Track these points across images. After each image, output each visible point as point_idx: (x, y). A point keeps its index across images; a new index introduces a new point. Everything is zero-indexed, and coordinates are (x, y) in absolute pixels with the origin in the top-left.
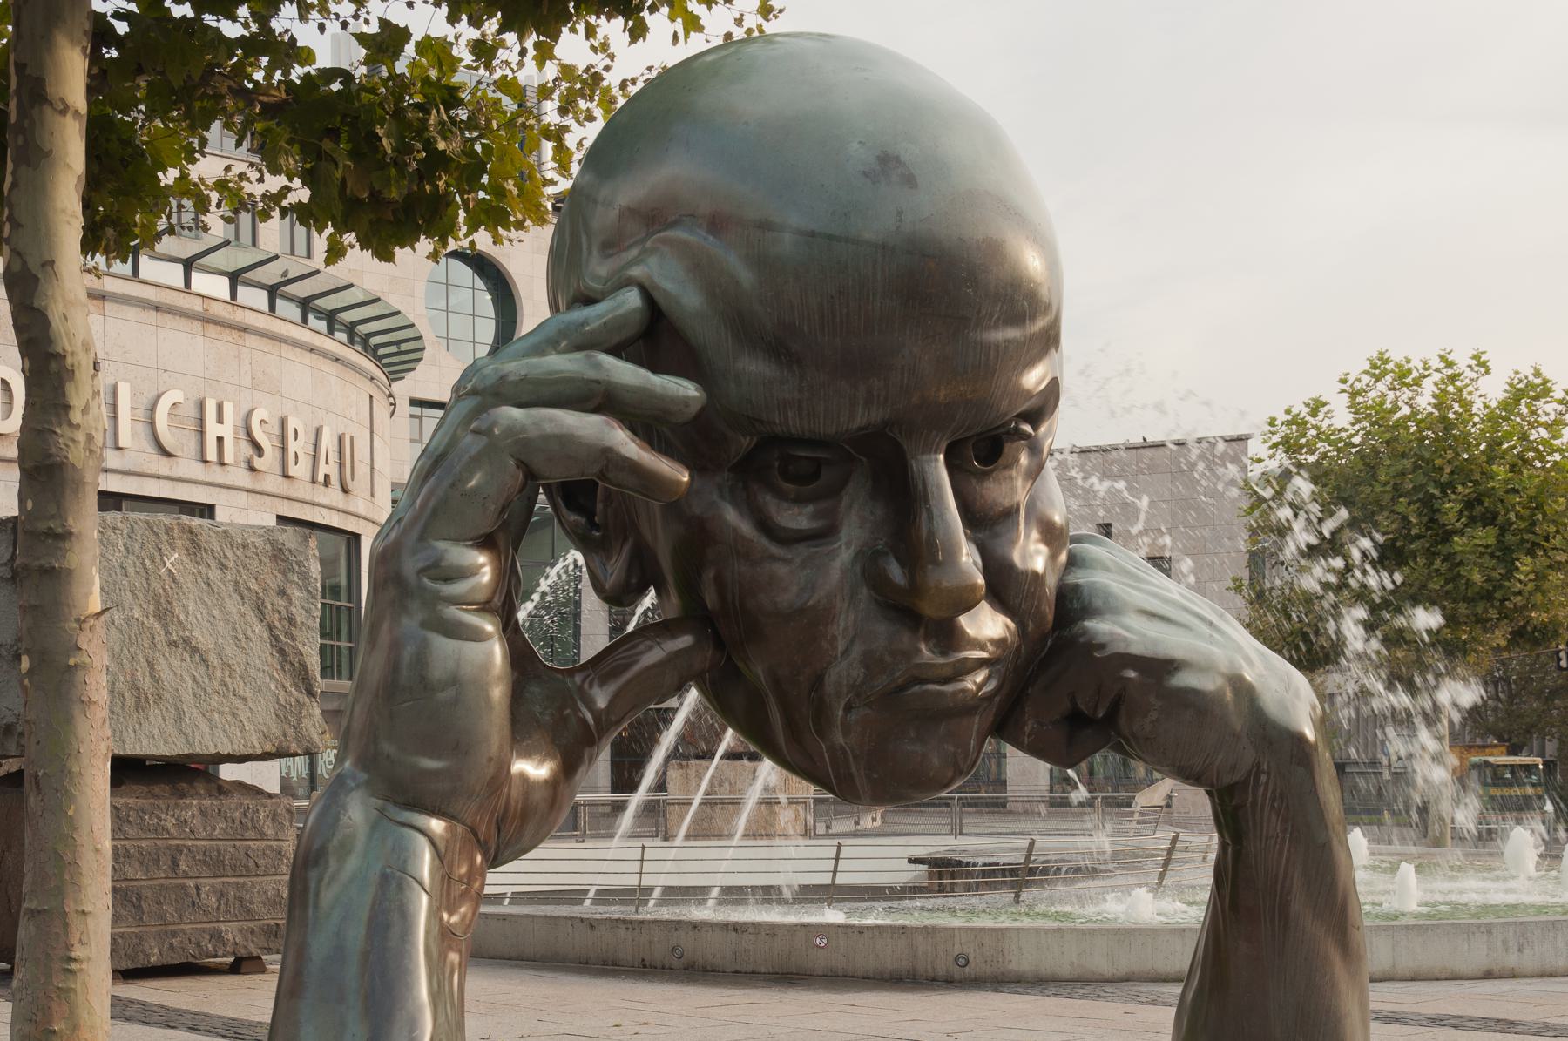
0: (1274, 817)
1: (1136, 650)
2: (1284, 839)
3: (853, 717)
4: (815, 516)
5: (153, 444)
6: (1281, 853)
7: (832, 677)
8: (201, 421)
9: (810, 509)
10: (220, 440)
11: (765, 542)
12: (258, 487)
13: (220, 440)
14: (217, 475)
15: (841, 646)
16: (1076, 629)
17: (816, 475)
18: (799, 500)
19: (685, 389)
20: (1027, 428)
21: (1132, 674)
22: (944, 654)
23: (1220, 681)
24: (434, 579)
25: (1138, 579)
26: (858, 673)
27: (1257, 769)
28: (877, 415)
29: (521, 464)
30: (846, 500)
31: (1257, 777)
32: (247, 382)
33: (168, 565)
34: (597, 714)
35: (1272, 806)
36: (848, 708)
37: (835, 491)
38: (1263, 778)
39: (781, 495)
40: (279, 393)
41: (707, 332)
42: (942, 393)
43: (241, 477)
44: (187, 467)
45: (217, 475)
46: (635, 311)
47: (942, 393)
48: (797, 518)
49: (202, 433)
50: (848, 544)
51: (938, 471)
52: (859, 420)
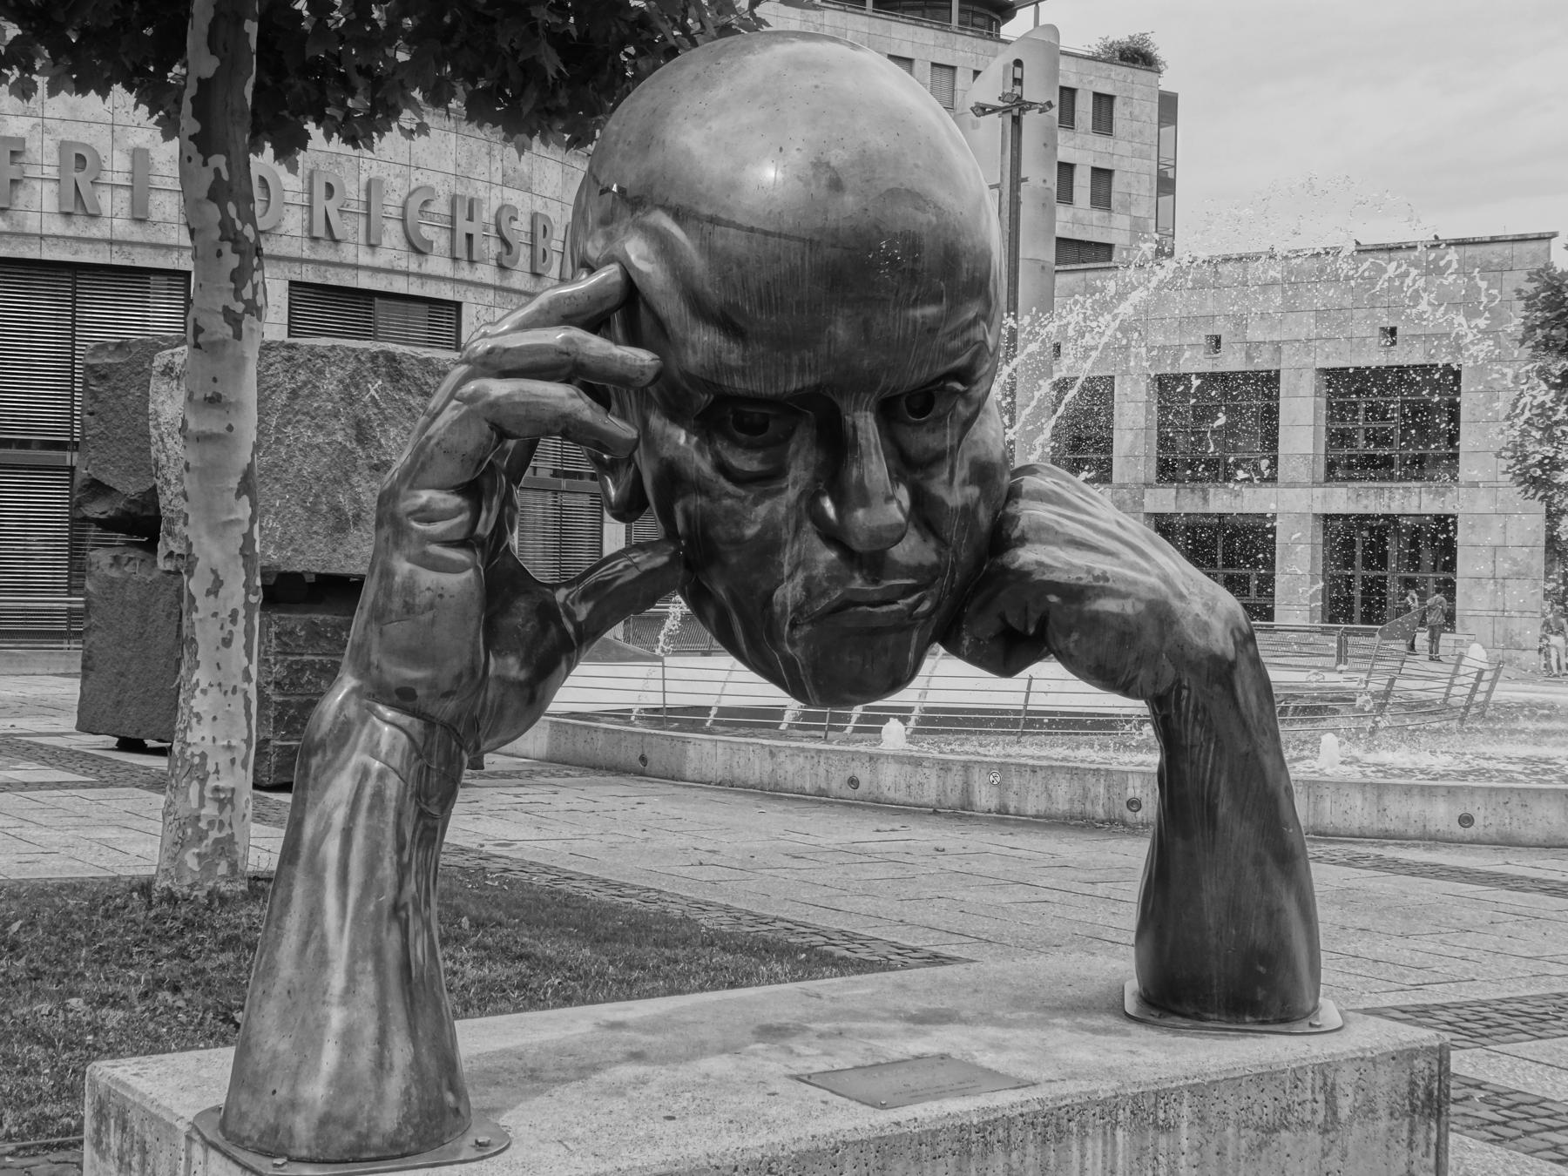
0: (1198, 729)
1: (1061, 577)
2: (1208, 749)
3: (797, 634)
4: (762, 461)
5: (404, 241)
6: (1206, 762)
7: (778, 594)
8: (453, 219)
9: (760, 455)
10: (469, 237)
11: (722, 481)
12: (505, 284)
13: (469, 237)
14: (465, 273)
15: (786, 570)
16: (1006, 558)
17: (763, 428)
18: (750, 447)
19: (642, 357)
20: (959, 386)
21: (1053, 599)
22: (876, 582)
23: (1141, 607)
24: (420, 521)
25: (1077, 509)
26: (799, 593)
27: (1178, 685)
28: (810, 380)
29: (494, 426)
30: (793, 447)
31: (1179, 694)
32: (498, 179)
33: (372, 392)
34: (577, 626)
35: (1195, 718)
36: (793, 625)
37: (783, 440)
38: (1185, 693)
39: (735, 443)
40: (529, 190)
41: (672, 307)
42: (866, 362)
43: (486, 273)
44: (438, 264)
45: (465, 273)
46: (614, 284)
47: (866, 362)
48: (747, 463)
49: (453, 230)
50: (795, 483)
51: (866, 425)
52: (795, 384)
